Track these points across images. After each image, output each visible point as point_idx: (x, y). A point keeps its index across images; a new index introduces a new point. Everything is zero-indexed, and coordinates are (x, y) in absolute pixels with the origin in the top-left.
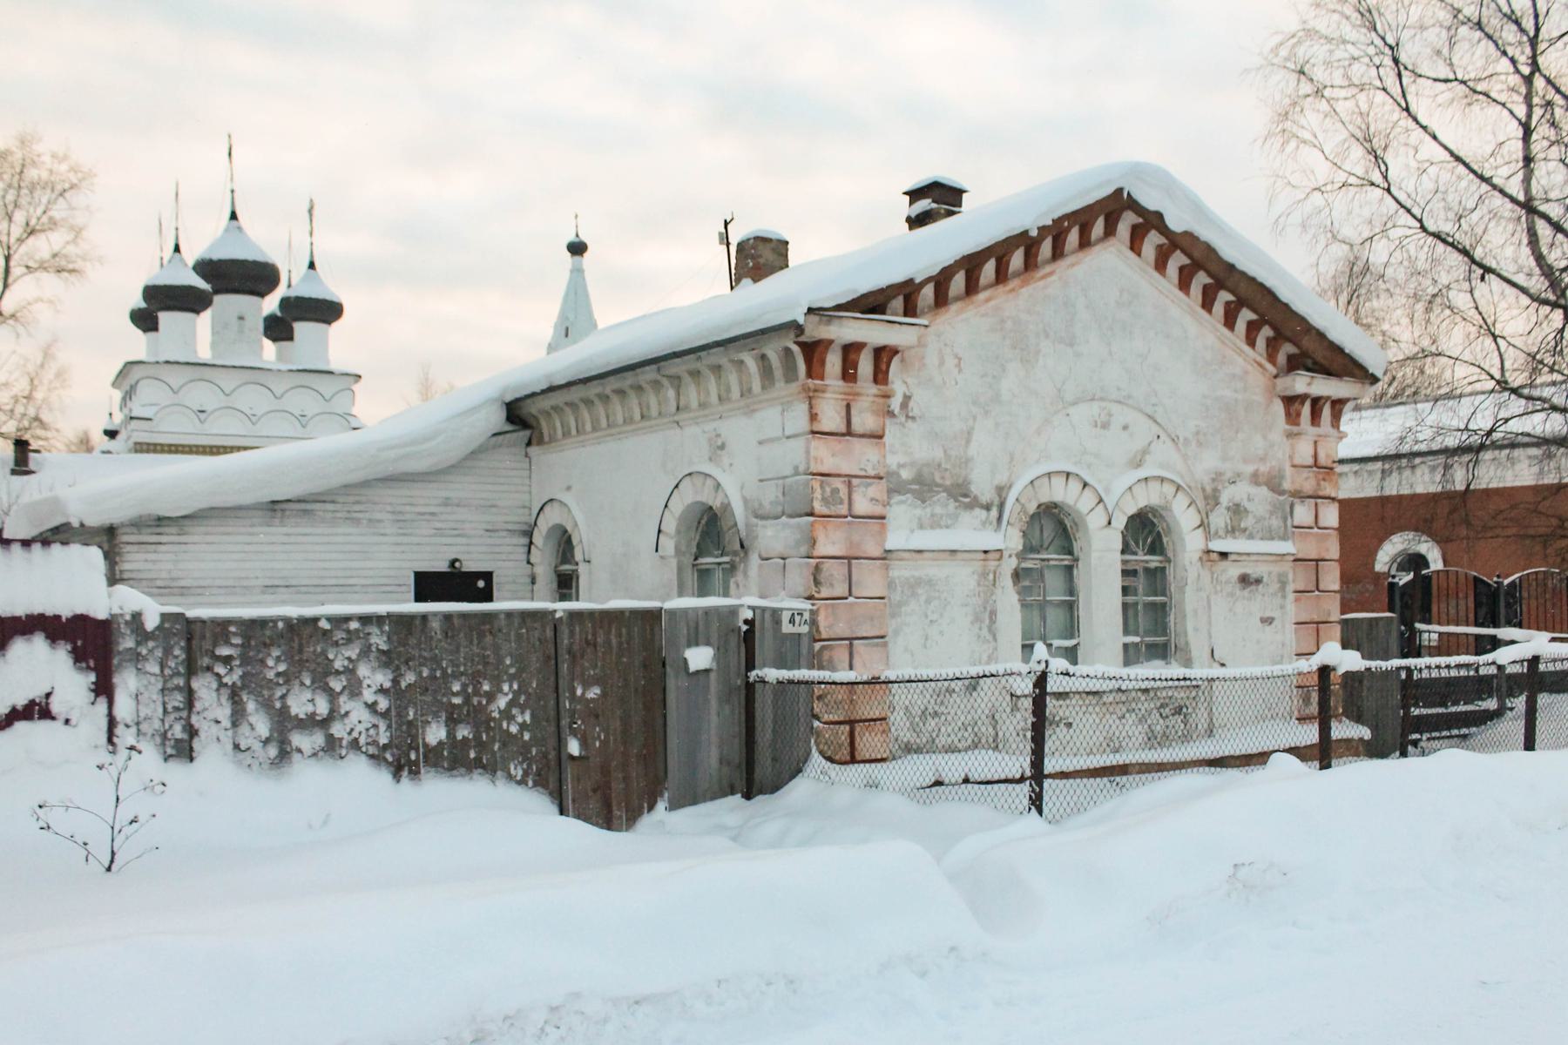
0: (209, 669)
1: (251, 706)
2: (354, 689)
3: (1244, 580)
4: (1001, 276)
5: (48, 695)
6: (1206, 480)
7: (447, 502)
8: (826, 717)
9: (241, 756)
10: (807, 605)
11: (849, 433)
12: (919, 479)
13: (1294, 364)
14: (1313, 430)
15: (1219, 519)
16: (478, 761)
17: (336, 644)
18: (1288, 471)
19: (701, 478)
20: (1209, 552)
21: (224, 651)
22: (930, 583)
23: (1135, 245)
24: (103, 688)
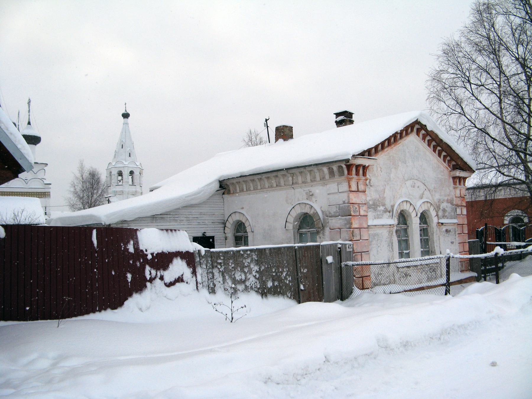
0: (216, 266)
1: (227, 277)
2: (250, 271)
3: (447, 231)
4: (389, 145)
5: (182, 275)
6: (437, 202)
7: (201, 214)
8: (357, 276)
9: (226, 292)
10: (350, 243)
11: (358, 191)
12: (374, 204)
13: (455, 168)
14: (460, 186)
15: (440, 213)
16: (280, 291)
17: (245, 258)
18: (455, 198)
19: (304, 205)
20: (439, 223)
21: (220, 261)
22: (378, 235)
23: (418, 134)
24: (194, 273)
